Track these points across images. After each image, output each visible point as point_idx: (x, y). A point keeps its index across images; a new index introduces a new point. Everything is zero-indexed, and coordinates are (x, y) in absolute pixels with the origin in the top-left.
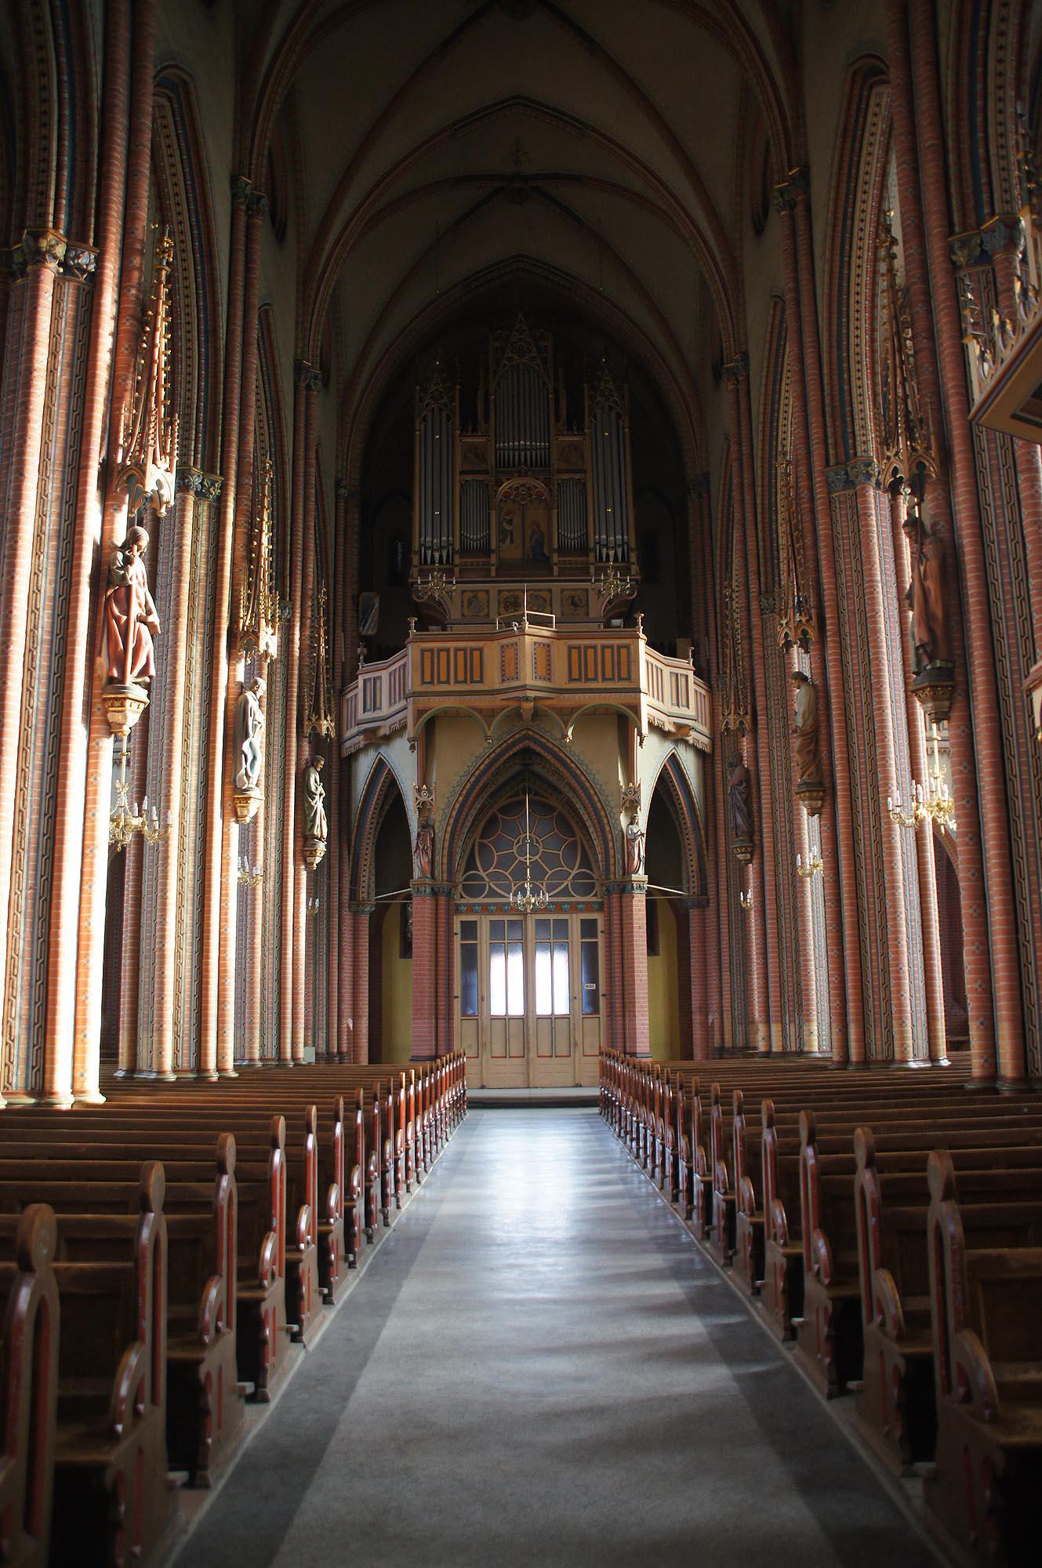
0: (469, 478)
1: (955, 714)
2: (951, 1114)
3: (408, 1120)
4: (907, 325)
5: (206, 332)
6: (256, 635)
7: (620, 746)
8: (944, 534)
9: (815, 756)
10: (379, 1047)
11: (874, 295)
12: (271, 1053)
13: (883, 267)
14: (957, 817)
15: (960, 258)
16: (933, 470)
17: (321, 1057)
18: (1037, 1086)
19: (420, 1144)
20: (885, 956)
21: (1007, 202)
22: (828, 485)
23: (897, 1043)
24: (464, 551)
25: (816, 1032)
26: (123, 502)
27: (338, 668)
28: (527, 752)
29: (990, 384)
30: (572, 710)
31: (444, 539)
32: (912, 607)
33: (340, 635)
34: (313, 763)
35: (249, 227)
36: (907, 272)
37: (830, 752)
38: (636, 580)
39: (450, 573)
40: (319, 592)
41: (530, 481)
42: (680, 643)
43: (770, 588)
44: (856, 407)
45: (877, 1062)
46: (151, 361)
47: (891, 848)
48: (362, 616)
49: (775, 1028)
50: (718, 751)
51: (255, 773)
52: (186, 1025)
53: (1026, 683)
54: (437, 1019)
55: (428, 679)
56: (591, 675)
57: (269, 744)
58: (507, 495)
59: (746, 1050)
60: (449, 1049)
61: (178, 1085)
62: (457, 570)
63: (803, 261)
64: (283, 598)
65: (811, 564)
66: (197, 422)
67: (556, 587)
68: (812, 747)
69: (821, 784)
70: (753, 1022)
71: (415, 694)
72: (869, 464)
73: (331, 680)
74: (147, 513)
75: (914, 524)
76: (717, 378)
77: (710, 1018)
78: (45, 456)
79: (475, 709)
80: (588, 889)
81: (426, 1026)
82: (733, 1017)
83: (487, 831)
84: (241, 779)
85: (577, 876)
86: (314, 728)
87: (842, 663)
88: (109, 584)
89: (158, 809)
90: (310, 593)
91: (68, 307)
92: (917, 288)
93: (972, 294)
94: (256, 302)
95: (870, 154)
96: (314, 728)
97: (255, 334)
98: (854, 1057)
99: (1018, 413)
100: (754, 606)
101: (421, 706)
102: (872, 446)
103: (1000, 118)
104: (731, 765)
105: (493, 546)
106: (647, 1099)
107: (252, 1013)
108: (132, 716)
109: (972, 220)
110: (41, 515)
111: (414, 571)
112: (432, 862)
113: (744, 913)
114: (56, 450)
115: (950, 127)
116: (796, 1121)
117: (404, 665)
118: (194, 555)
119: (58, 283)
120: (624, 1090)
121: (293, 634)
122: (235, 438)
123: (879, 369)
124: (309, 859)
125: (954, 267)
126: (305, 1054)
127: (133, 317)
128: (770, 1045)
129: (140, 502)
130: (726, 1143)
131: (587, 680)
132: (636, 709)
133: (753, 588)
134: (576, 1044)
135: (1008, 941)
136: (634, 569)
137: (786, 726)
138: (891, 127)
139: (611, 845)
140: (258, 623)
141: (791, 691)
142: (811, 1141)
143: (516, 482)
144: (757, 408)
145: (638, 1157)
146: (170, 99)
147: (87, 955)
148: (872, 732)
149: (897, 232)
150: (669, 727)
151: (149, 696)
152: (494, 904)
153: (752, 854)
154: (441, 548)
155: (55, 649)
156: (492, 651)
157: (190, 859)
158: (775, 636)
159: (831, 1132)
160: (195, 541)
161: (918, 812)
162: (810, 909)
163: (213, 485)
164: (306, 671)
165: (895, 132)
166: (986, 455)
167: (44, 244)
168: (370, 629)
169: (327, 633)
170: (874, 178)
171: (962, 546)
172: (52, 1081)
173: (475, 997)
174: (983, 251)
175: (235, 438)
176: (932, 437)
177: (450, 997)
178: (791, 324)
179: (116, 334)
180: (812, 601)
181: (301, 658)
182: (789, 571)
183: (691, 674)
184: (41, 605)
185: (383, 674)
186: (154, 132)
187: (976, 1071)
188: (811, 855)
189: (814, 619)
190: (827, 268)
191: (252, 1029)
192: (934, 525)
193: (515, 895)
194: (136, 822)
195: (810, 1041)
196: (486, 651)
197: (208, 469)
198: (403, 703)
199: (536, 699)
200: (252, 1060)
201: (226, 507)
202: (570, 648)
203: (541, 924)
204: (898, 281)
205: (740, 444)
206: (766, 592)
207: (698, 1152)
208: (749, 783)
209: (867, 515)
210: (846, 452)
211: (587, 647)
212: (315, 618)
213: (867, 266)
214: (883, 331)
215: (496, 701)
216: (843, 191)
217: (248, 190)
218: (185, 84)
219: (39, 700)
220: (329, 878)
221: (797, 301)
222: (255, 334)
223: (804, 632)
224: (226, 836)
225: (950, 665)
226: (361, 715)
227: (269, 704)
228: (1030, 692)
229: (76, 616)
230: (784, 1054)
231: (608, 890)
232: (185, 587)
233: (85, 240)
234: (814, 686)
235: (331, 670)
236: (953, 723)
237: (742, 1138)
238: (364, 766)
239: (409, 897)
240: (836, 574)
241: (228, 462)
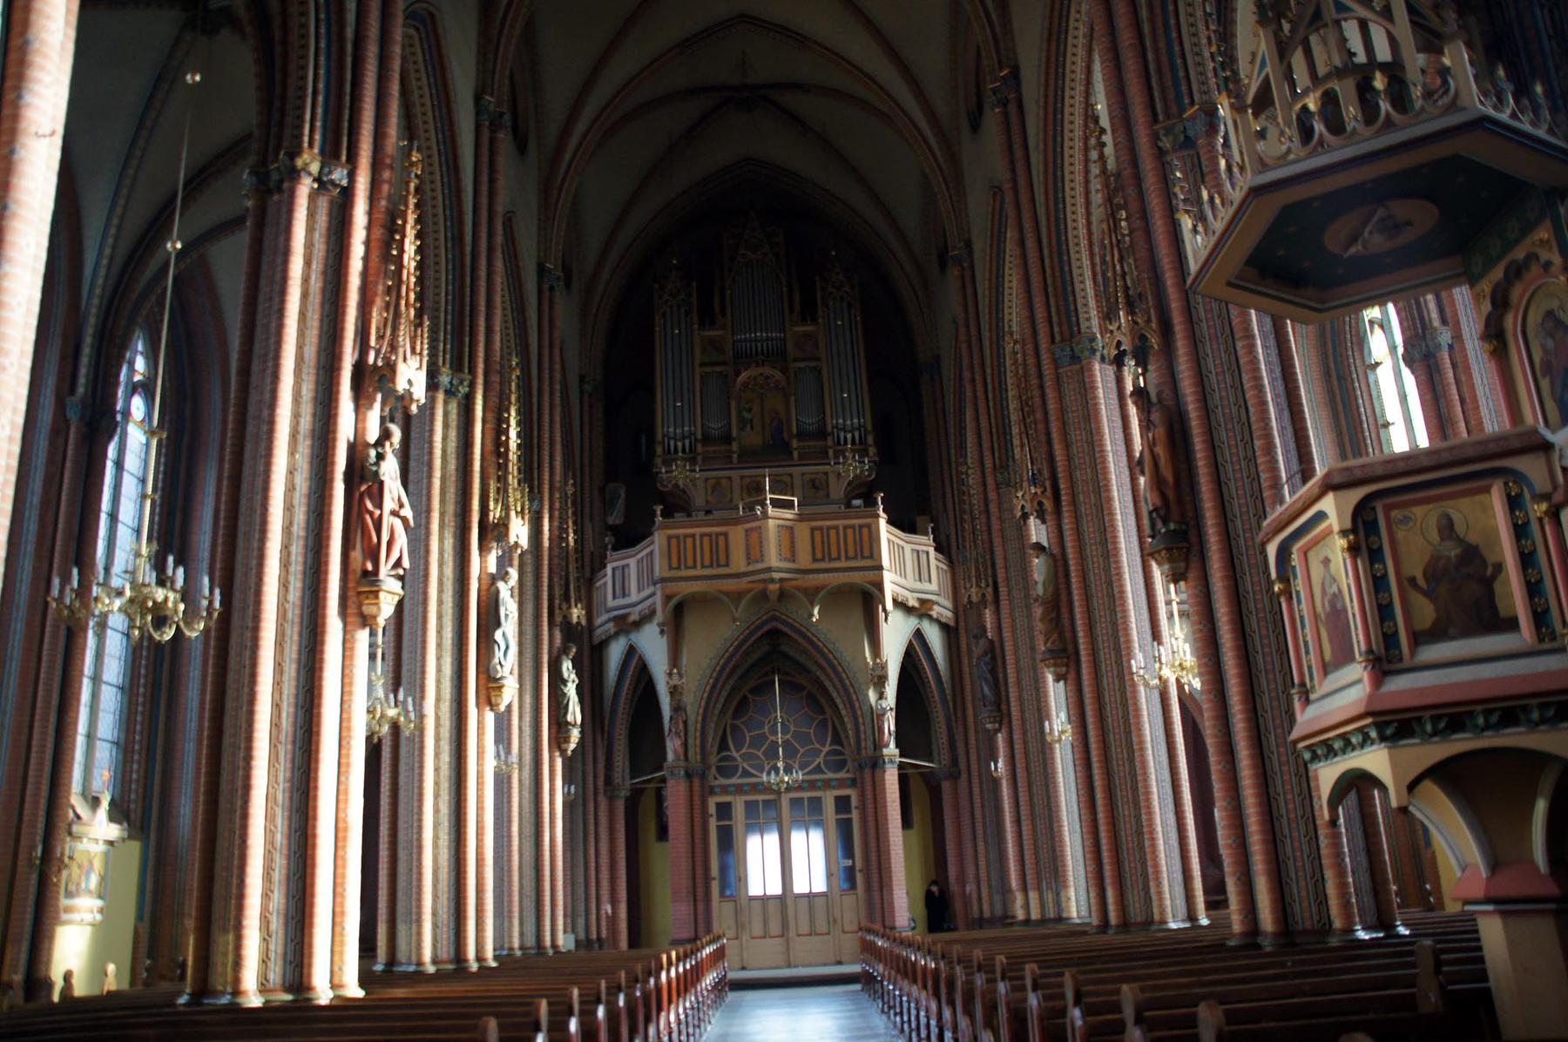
0: (708, 369)
1: (1191, 575)
2: (1216, 971)
3: (670, 1002)
4: (1120, 207)
5: (453, 239)
6: (506, 527)
7: (865, 622)
8: (1170, 403)
9: (1057, 625)
10: (639, 933)
11: (1087, 182)
12: (530, 941)
13: (1094, 155)
14: (1200, 675)
15: (1166, 143)
16: (1154, 341)
17: (584, 944)
18: (1299, 940)
19: (683, 1027)
20: (1138, 818)
21: (1205, 93)
22: (1056, 363)
23: (1155, 904)
24: (707, 439)
25: (1073, 898)
26: (375, 400)
27: (587, 560)
28: (774, 634)
29: (1204, 254)
30: (818, 589)
31: (686, 429)
32: (1143, 473)
33: (588, 525)
34: (564, 651)
35: (492, 141)
36: (1117, 158)
37: (1072, 620)
38: (874, 462)
39: (693, 461)
40: (566, 484)
41: (767, 370)
42: (920, 520)
43: (1004, 463)
44: (1078, 286)
45: (1136, 924)
46: (400, 266)
47: (1137, 710)
48: (608, 505)
49: (1033, 895)
50: (962, 624)
51: (507, 663)
52: (445, 915)
53: (1261, 535)
54: (695, 900)
55: (675, 564)
56: (834, 555)
57: (521, 634)
58: (745, 384)
59: (1006, 919)
60: (709, 930)
61: (439, 976)
62: (699, 458)
63: (1019, 154)
64: (531, 491)
65: (1043, 438)
66: (446, 323)
67: (796, 471)
68: (1054, 615)
69: (1064, 650)
70: (1010, 891)
71: (663, 580)
72: (1093, 339)
73: (580, 569)
74: (399, 409)
75: (1139, 393)
76: (943, 265)
77: (968, 889)
78: (300, 358)
79: (721, 592)
80: (840, 765)
81: (684, 909)
82: (990, 887)
83: (741, 708)
84: (495, 668)
85: (828, 753)
86: (565, 617)
87: (1078, 532)
88: (363, 480)
89: (414, 700)
90: (558, 485)
91: (322, 219)
92: (1128, 172)
93: (1182, 172)
94: (500, 209)
95: (1074, 55)
96: (565, 617)
97: (499, 239)
98: (1113, 918)
99: (1233, 280)
100: (990, 481)
101: (668, 591)
102: (1095, 322)
103: (1191, 20)
104: (975, 637)
105: (734, 433)
106: (908, 972)
107: (510, 902)
108: (386, 608)
109: (1174, 110)
110: (296, 416)
111: (658, 461)
112: (685, 745)
113: (996, 782)
114: (311, 351)
115: (1146, 28)
116: (1061, 985)
117: (652, 553)
118: (444, 451)
119: (312, 197)
120: (886, 965)
121: (542, 526)
122: (482, 338)
123: (1096, 250)
124: (564, 746)
125: (1160, 153)
126: (565, 941)
127: (383, 226)
128: (1028, 913)
129: (392, 400)
130: (991, 1009)
131: (831, 559)
132: (880, 586)
133: (988, 463)
134: (835, 921)
135: (1259, 795)
136: (872, 451)
137: (1027, 596)
138: (1092, 29)
139: (861, 720)
140: (508, 516)
141: (1030, 562)
142: (1077, 1003)
143: (752, 372)
144: (983, 289)
145: (902, 1031)
146: (417, 29)
147: (347, 772)
148: (1112, 597)
149: (1105, 122)
150: (912, 603)
151: (403, 588)
152: (748, 784)
153: (1001, 723)
154: (683, 438)
155: (311, 543)
156: (737, 534)
157: (446, 748)
158: (1011, 510)
159: (1097, 994)
160: (445, 438)
161: (1162, 673)
162: (1060, 775)
163: (461, 382)
164: (556, 561)
165: (1096, 35)
166: (1204, 324)
167: (299, 163)
168: (615, 518)
169: (575, 523)
170: (1080, 76)
171: (1187, 412)
172: (309, 976)
173: (732, 878)
174: (1187, 137)
175: (482, 338)
176: (1152, 311)
177: (707, 879)
178: (1011, 212)
179: (367, 243)
180: (1046, 473)
181: (550, 548)
182: (1022, 445)
183: (931, 550)
184: (296, 502)
185: (631, 562)
186: (404, 59)
187: (1237, 927)
188: (1059, 723)
189: (1049, 490)
190: (1041, 157)
191: (510, 918)
192: (1159, 394)
193: (769, 774)
194: (392, 712)
195: (1068, 907)
196: (731, 537)
197: (457, 367)
198: (651, 589)
199: (781, 580)
200: (511, 949)
201: (474, 404)
202: (813, 530)
203: (796, 803)
204: (1109, 167)
205: (968, 326)
206: (1001, 467)
207: (963, 1022)
208: (994, 654)
209: (1094, 388)
210: (1070, 328)
211: (829, 528)
212: (563, 510)
213: (1078, 156)
214: (1098, 213)
215: (742, 584)
216: (1052, 88)
217: (492, 107)
218: (432, 15)
219: (294, 595)
220: (584, 764)
221: (1015, 189)
222: (499, 239)
223: (1040, 504)
224: (481, 726)
225: (1184, 527)
226: (611, 603)
227: (521, 595)
228: (1263, 545)
229: (330, 513)
230: (1043, 921)
231: (860, 765)
232: (437, 483)
233: (337, 156)
234: (1052, 555)
235: (580, 559)
236: (1192, 584)
237: (1008, 1004)
238: (616, 652)
239: (663, 780)
240: (1067, 446)
241: (477, 335)
